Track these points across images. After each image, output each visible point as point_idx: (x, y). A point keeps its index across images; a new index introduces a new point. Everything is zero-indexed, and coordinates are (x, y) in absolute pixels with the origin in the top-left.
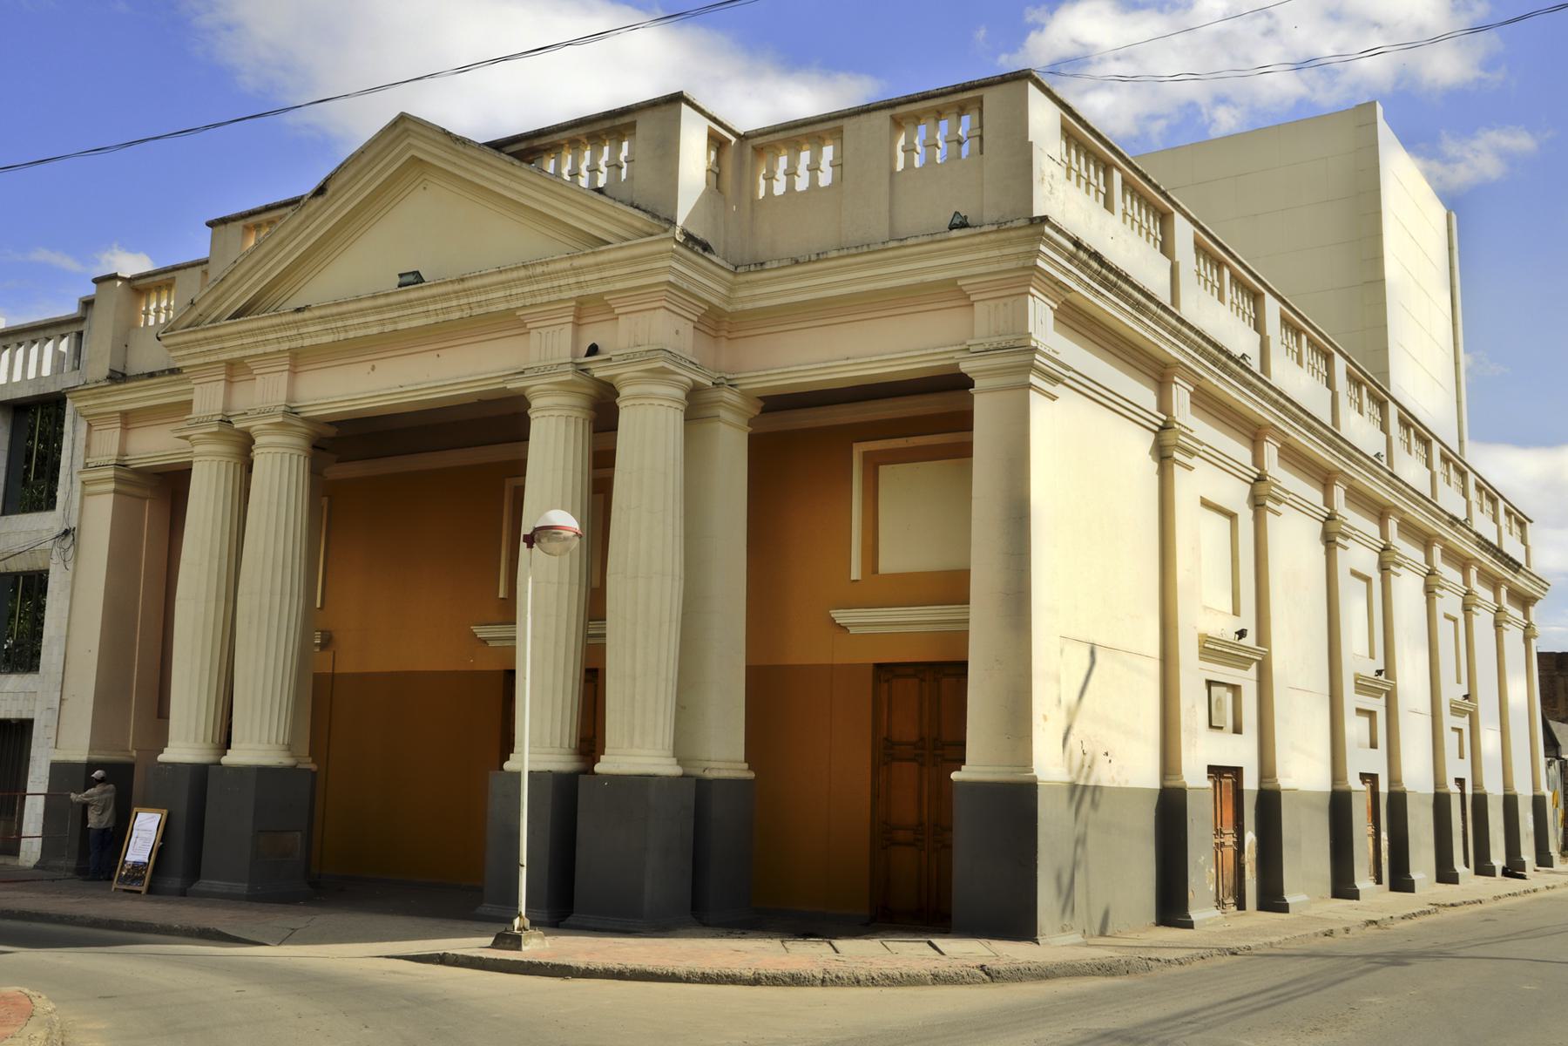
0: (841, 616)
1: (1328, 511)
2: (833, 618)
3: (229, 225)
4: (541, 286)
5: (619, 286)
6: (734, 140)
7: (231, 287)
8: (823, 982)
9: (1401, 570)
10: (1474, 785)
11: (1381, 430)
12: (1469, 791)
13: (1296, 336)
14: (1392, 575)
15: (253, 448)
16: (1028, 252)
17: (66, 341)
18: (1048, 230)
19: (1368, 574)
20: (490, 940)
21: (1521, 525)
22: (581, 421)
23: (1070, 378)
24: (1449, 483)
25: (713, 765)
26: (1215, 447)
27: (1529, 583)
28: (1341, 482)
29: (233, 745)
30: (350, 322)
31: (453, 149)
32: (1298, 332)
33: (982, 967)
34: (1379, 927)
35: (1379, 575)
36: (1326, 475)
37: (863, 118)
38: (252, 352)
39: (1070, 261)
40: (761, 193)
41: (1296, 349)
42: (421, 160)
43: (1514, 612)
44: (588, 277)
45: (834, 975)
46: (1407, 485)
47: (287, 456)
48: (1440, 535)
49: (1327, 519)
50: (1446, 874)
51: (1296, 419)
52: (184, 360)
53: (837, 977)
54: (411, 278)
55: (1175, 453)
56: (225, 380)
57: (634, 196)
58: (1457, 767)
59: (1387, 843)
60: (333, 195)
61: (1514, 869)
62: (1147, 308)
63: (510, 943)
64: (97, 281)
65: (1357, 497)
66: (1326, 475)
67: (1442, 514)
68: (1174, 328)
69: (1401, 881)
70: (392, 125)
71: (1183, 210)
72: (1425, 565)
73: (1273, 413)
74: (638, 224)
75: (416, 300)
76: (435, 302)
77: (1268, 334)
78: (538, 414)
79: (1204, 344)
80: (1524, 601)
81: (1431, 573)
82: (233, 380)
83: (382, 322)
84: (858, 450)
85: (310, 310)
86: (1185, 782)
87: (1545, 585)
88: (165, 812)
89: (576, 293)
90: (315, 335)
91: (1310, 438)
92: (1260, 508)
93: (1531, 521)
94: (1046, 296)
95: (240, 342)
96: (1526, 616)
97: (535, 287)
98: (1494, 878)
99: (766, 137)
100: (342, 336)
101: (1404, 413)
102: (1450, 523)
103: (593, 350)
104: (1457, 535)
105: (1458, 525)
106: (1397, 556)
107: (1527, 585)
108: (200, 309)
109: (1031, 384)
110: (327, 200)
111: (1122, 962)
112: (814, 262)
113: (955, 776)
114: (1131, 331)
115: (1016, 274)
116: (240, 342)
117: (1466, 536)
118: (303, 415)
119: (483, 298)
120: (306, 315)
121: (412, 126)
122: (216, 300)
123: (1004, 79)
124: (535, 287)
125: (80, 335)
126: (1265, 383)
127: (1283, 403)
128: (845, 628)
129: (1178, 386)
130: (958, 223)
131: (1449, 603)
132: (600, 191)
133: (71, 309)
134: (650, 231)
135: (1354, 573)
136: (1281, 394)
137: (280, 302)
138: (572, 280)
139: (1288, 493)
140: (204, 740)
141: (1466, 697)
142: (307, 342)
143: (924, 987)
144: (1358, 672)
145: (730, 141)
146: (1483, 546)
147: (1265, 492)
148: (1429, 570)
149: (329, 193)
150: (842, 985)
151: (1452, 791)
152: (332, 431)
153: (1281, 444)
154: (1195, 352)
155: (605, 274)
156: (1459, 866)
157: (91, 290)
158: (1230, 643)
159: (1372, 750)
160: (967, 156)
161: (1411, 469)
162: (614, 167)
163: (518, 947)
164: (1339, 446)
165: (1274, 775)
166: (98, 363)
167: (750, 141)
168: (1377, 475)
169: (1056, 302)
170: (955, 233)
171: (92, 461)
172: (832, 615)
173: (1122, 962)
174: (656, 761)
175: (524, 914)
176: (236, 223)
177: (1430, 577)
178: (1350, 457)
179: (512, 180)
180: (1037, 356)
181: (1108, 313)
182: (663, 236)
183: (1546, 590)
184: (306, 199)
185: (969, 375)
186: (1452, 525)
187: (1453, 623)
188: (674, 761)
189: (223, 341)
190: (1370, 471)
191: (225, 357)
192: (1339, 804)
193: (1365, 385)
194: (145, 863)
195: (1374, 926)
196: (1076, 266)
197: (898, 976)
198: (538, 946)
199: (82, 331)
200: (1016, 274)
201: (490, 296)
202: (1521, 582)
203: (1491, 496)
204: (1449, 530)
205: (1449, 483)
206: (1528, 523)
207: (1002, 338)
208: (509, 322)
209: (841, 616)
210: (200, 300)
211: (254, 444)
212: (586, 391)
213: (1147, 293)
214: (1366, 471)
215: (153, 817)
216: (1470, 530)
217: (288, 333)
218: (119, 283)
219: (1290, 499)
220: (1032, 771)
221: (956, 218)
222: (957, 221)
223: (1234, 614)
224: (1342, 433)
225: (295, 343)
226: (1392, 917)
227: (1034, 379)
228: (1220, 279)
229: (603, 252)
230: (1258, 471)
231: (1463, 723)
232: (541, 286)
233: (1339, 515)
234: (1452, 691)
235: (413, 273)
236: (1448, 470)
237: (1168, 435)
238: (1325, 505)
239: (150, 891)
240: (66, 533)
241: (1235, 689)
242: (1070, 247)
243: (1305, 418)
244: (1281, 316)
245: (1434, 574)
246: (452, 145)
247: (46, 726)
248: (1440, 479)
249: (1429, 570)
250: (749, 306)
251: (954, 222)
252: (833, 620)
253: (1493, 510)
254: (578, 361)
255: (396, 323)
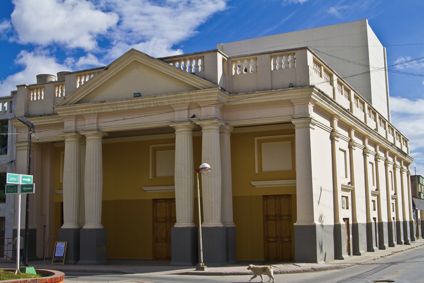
0: (254, 183)
1: (376, 153)
2: (251, 184)
3: (71, 75)
4: (179, 99)
5: (202, 100)
6: (227, 59)
7: (77, 94)
8: (280, 273)
9: (356, 148)
10: (396, 219)
11: (375, 121)
12: (377, 221)
13: (319, 67)
14: (378, 162)
15: (86, 140)
16: (309, 94)
17: (6, 103)
18: (314, 89)
19: (345, 150)
20: (195, 269)
21: (406, 142)
22: (190, 134)
23: (317, 124)
24: (342, 94)
25: (228, 223)
26: (322, 123)
27: (409, 159)
28: (353, 129)
29: (64, 223)
30: (118, 106)
31: (149, 60)
32: (320, 66)
33: (312, 268)
34: (384, 258)
35: (348, 150)
36: (364, 136)
37: (263, 55)
38: (85, 113)
39: (317, 95)
40: (234, 73)
41: (341, 90)
42: (137, 61)
43: (405, 168)
44: (193, 98)
45: (282, 271)
46: (382, 137)
47: (97, 142)
48: (389, 149)
49: (350, 141)
50: (370, 249)
51: (359, 124)
52: (62, 114)
53: (283, 272)
54: (138, 95)
55: (335, 138)
56: (75, 120)
57: (205, 76)
58: (374, 214)
59: (378, 236)
60: (110, 70)
61: (407, 243)
62: (331, 102)
63: (201, 269)
64: (17, 86)
65: (342, 124)
66: (364, 136)
67: (389, 143)
68: (336, 106)
69: (356, 252)
70: (129, 52)
71: (335, 73)
72: (385, 158)
73: (338, 112)
74: (208, 85)
75: (140, 101)
76: (146, 102)
77: (352, 101)
78: (177, 133)
79: (342, 109)
80: (407, 164)
81: (365, 148)
82: (77, 120)
83: (129, 106)
84: (256, 139)
85: (106, 102)
86: (340, 223)
87: (413, 159)
88: (67, 242)
89: (189, 101)
90: (106, 109)
91: (362, 128)
92: (351, 148)
93: (408, 140)
94: (312, 104)
95: (81, 110)
96: (408, 169)
97: (177, 99)
98: (373, 252)
99: (235, 59)
100: (116, 110)
101: (397, 131)
102: (391, 145)
103: (194, 116)
104: (392, 148)
105: (393, 146)
106: (379, 157)
107: (408, 160)
108: (67, 100)
109: (310, 127)
110: (108, 71)
111: (340, 266)
112: (252, 94)
113: (295, 224)
114: (332, 112)
115: (305, 99)
116: (81, 110)
117: (394, 148)
118: (102, 131)
119: (161, 101)
120: (104, 103)
121: (135, 52)
122: (73, 97)
123: (301, 49)
124: (177, 99)
125: (11, 102)
126: (387, 140)
127: (356, 120)
128: (254, 186)
129: (335, 120)
130: (291, 86)
131: (371, 158)
132: (194, 74)
133: (9, 94)
134: (212, 86)
135: (340, 149)
136: (356, 118)
137: (92, 97)
138: (188, 98)
139: (357, 144)
140: (75, 222)
141: (349, 183)
142: (104, 111)
143: (302, 273)
144: (372, 190)
145: (226, 60)
146: (398, 150)
147: (352, 144)
148: (386, 159)
149: (109, 69)
150: (285, 273)
151: (372, 222)
152: (107, 134)
153: (338, 120)
154: (339, 111)
155: (198, 97)
156: (375, 248)
157: (16, 89)
158: (346, 186)
159: (374, 211)
160: (291, 68)
161: (371, 124)
162: (197, 67)
163: (204, 270)
164: (368, 129)
165: (356, 220)
166: (20, 111)
167: (231, 59)
168: (375, 135)
169: (313, 105)
170: (290, 88)
171: (19, 140)
172: (251, 183)
173: (340, 266)
174: (217, 223)
175: (202, 262)
176: (74, 74)
177: (365, 150)
178: (370, 131)
179: (167, 70)
180: (312, 120)
181: (327, 108)
182: (216, 88)
183: (413, 160)
184: (40, 48)
185: (294, 124)
186: (391, 146)
187: (344, 153)
188: (221, 223)
189: (75, 110)
190: (374, 134)
191: (76, 114)
192: (337, 228)
193: (323, 66)
194: (62, 257)
195: (383, 258)
196: (318, 96)
197: (296, 271)
198: (207, 270)
199: (12, 101)
200: (305, 99)
201: (163, 101)
202: (407, 159)
203: (399, 134)
204: (391, 147)
205: (358, 107)
206: (408, 141)
207: (302, 115)
208: (170, 109)
209: (254, 183)
210: (67, 98)
211: (86, 139)
212: (192, 127)
213: (343, 108)
214: (373, 134)
215: (62, 244)
216: (396, 146)
217: (98, 108)
218: (26, 87)
219: (341, 136)
220: (314, 222)
221: (290, 85)
222: (291, 85)
223: (346, 177)
224: (368, 125)
225: (100, 111)
226: (386, 255)
227: (311, 125)
228: (321, 70)
229: (198, 91)
230: (350, 139)
231: (375, 198)
232: (179, 99)
233: (336, 130)
234: (372, 188)
235: (138, 93)
236: (357, 102)
237: (333, 133)
238: (375, 151)
239: (65, 264)
240: (12, 162)
241: (347, 198)
242: (318, 91)
243: (361, 123)
244: (354, 95)
245: (387, 160)
246: (149, 58)
247: (10, 219)
248: (368, 116)
249: (386, 159)
250: (233, 104)
251: (290, 86)
252: (251, 184)
253: (374, 117)
254: (190, 119)
255: (133, 107)
